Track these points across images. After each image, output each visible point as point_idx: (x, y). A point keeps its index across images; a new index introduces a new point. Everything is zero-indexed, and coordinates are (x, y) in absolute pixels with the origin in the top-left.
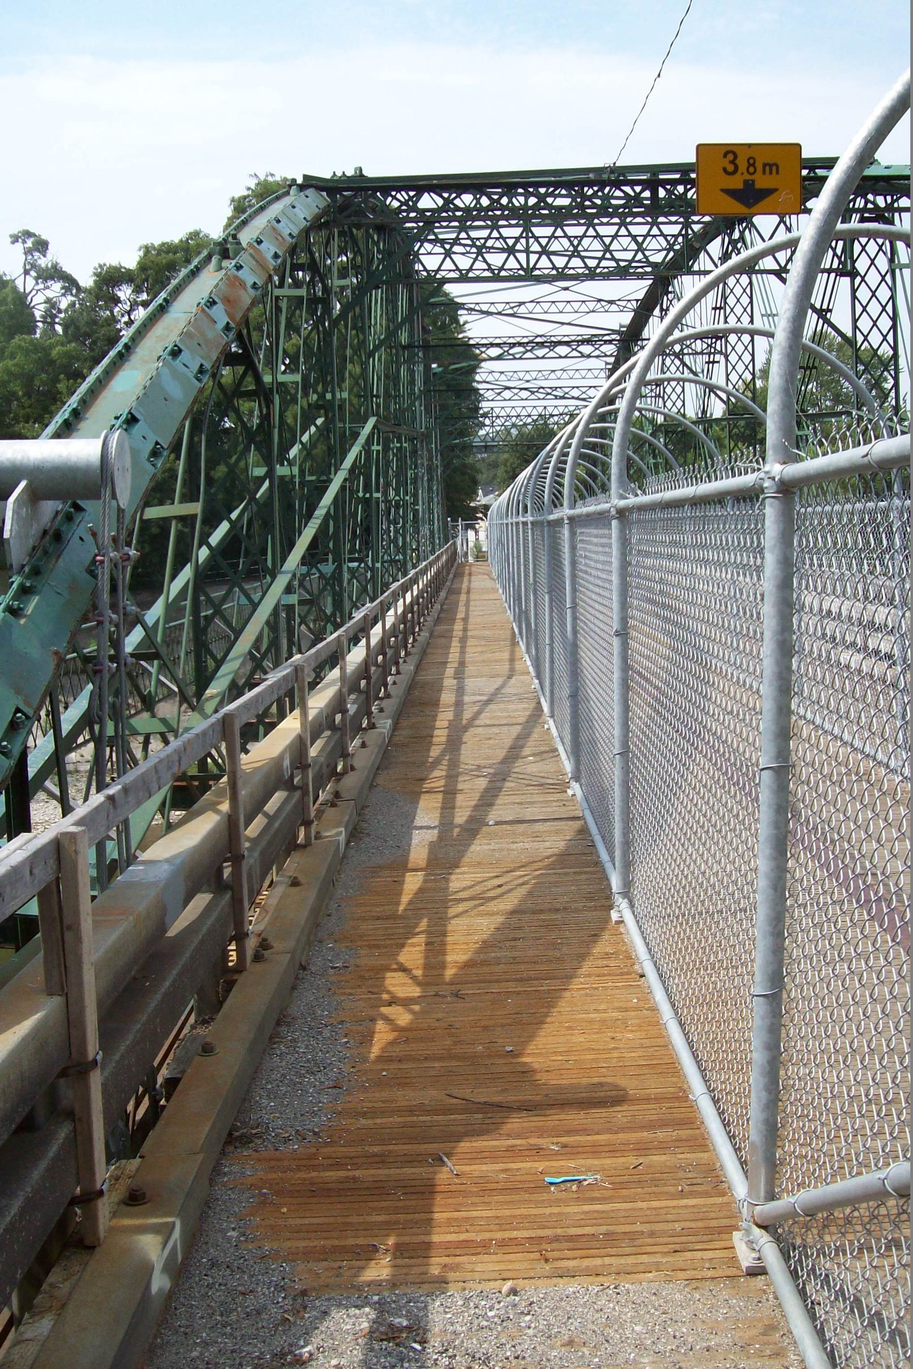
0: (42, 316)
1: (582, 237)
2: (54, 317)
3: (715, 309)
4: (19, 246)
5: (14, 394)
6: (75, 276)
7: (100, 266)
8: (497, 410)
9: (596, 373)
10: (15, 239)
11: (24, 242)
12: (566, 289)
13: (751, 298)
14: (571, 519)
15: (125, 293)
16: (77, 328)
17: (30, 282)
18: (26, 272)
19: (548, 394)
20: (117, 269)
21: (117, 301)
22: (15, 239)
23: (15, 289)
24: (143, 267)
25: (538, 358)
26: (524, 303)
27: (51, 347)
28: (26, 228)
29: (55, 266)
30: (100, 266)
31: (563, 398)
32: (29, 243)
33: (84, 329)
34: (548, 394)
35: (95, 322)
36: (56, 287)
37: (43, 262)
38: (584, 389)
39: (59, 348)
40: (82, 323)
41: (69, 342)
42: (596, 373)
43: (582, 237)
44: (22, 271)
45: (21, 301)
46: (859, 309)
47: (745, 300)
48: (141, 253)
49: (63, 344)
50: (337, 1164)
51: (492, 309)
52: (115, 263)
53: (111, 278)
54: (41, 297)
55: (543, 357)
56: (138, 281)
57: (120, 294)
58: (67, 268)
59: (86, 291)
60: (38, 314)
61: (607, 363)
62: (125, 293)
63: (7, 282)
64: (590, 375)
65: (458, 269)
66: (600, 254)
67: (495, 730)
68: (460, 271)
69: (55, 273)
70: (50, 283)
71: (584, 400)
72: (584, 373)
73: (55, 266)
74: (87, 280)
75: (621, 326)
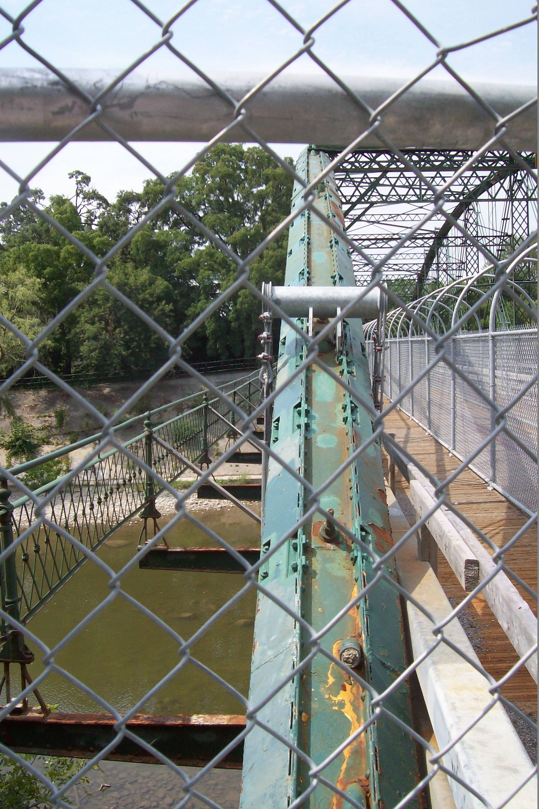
0: (86, 221)
1: (470, 177)
2: (92, 221)
3: (503, 219)
4: (74, 179)
5: (70, 265)
6: (106, 197)
7: (121, 192)
8: (359, 277)
9: (419, 255)
10: (71, 176)
11: (77, 177)
12: (421, 207)
13: (527, 213)
14: (411, 341)
15: (135, 207)
16: (108, 227)
17: (80, 199)
18: (78, 195)
19: (390, 268)
20: (131, 193)
21: (129, 211)
22: (71, 176)
23: (71, 204)
24: (146, 193)
25: (378, 248)
26: (398, 215)
27: (94, 238)
28: (78, 169)
29: (94, 192)
30: (121, 192)
31: (398, 270)
32: (80, 178)
33: (112, 228)
34: (390, 268)
35: (117, 224)
36: (95, 203)
37: (86, 189)
38: (410, 266)
39: (98, 239)
40: (109, 224)
41: (104, 235)
42: (419, 255)
43: (470, 177)
44: (75, 193)
45: (74, 210)
46: (514, 220)
47: (524, 215)
48: (145, 185)
49: (100, 236)
50: (500, 660)
51: (404, 217)
52: (129, 190)
53: (127, 199)
54: (85, 208)
55: (381, 247)
56: (143, 200)
57: (132, 208)
58: (102, 193)
59: (114, 206)
60: (83, 220)
61: (425, 250)
62: (135, 207)
63: (66, 200)
64: (415, 257)
65: (398, 195)
66: (361, 185)
67: (426, 456)
68: (399, 196)
69: (94, 196)
70: (91, 201)
71: (410, 271)
72: (411, 256)
73: (94, 192)
74: (113, 200)
75: (436, 229)
